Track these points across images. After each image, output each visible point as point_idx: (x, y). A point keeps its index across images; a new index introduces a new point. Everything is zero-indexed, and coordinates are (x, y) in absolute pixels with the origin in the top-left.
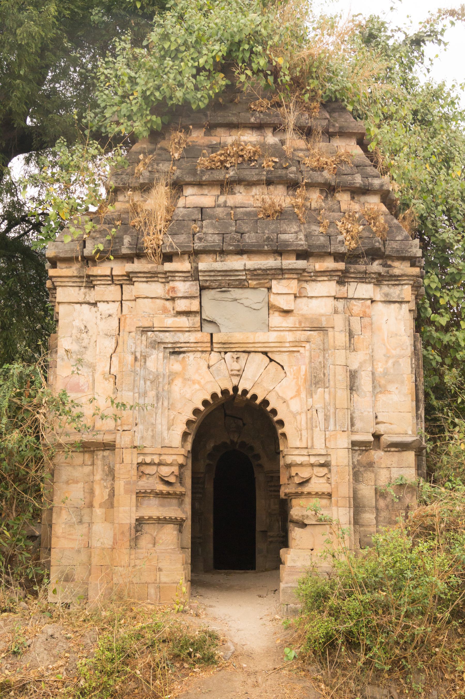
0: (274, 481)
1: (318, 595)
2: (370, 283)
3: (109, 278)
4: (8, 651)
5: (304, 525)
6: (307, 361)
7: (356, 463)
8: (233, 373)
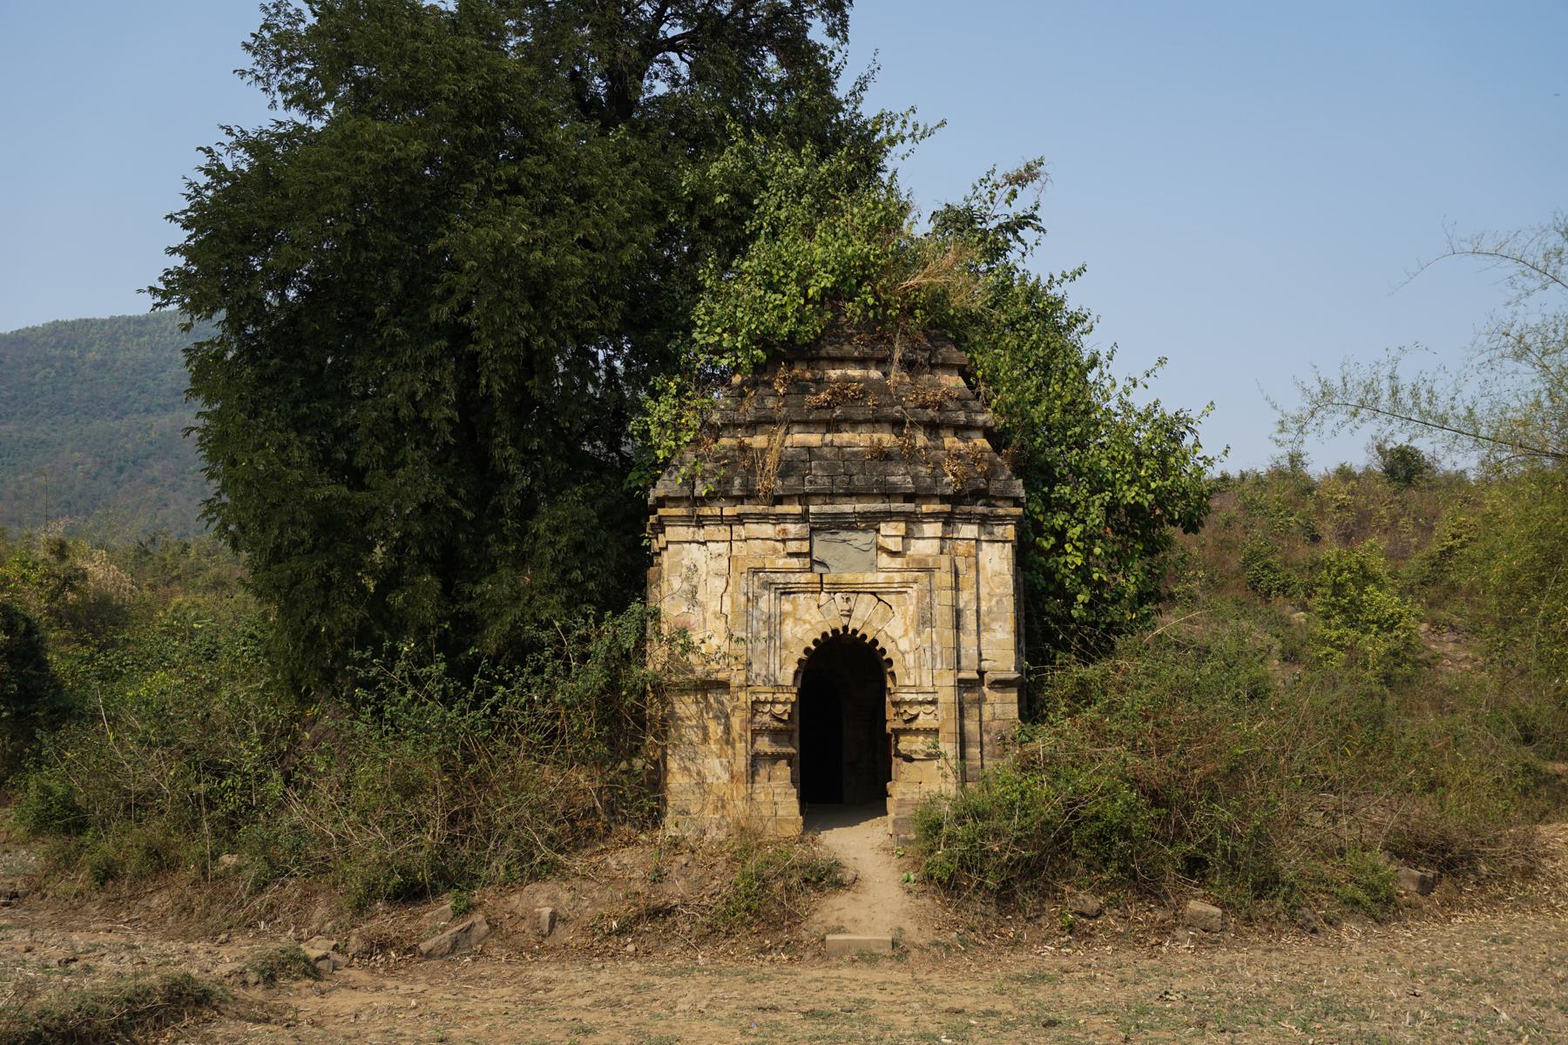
5: (909, 759)
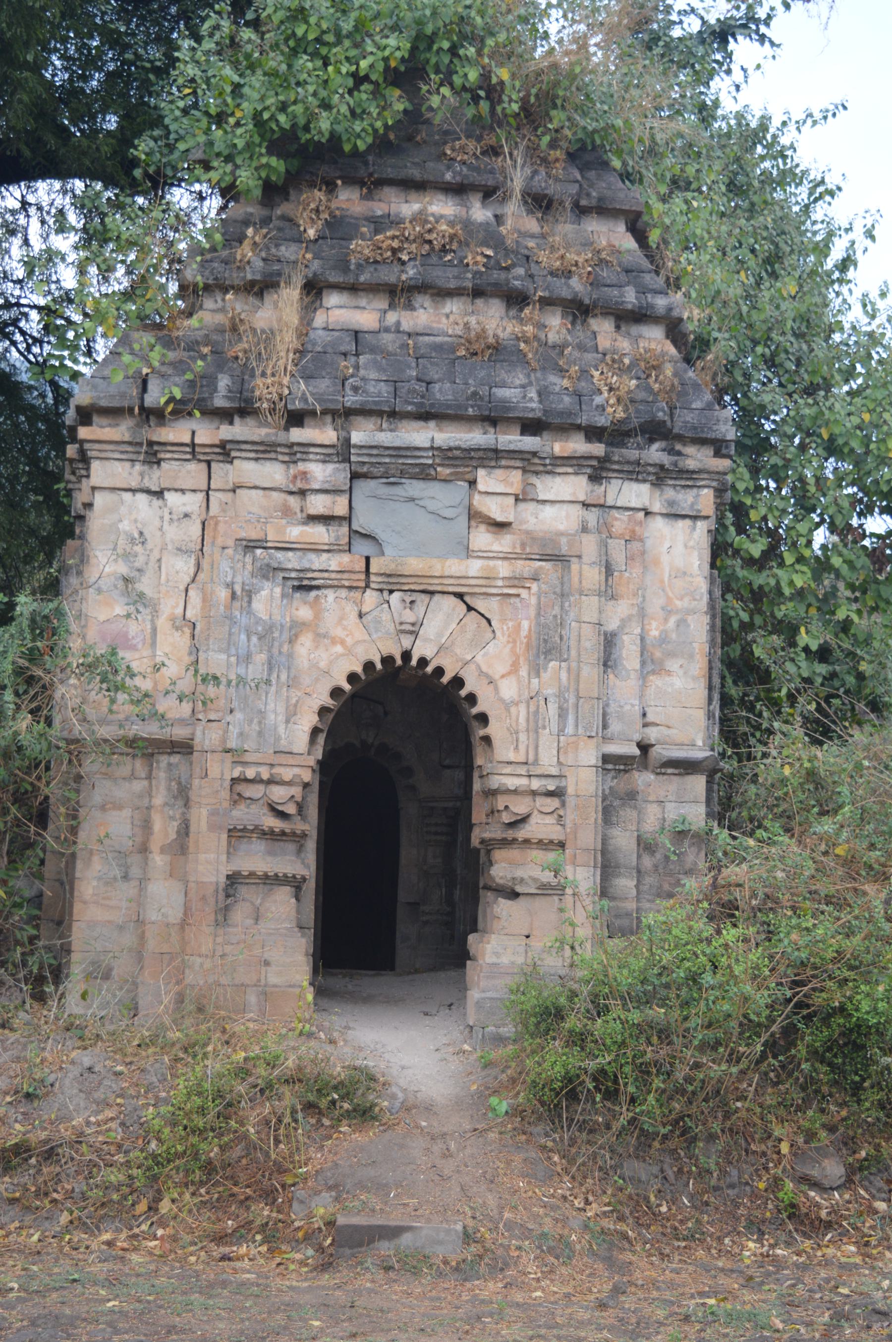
0: (456, 816)
1: (546, 1012)
2: (644, 481)
3: (188, 449)
4: (16, 1092)
5: (514, 895)
6: (532, 612)
7: (607, 792)
8: (403, 627)
